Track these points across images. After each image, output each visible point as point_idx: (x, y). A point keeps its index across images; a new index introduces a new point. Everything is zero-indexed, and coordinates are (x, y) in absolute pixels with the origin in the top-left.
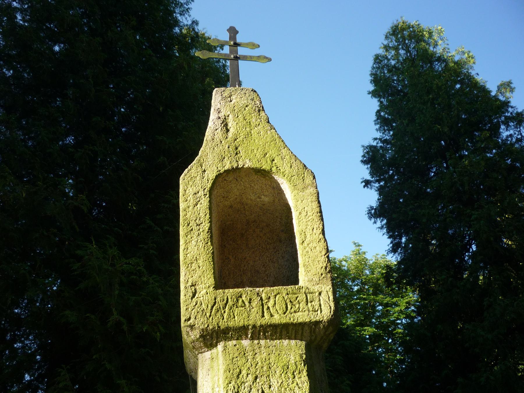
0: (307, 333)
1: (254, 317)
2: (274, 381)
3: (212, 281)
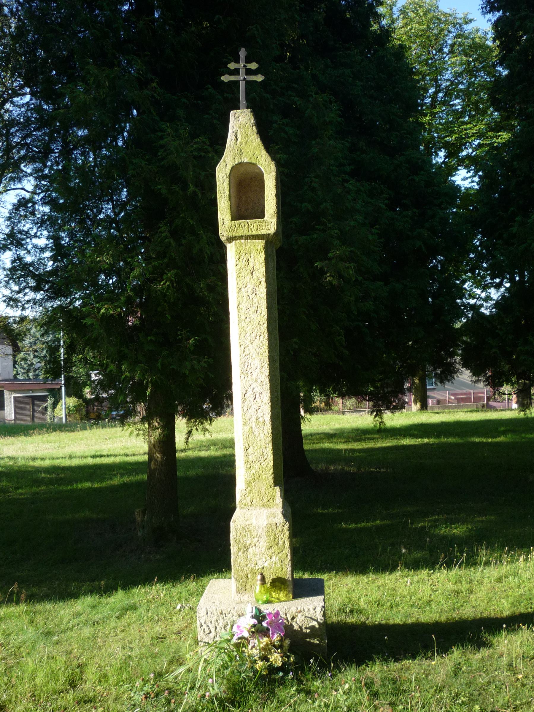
0: (265, 238)
1: (246, 233)
2: (252, 255)
3: (230, 218)
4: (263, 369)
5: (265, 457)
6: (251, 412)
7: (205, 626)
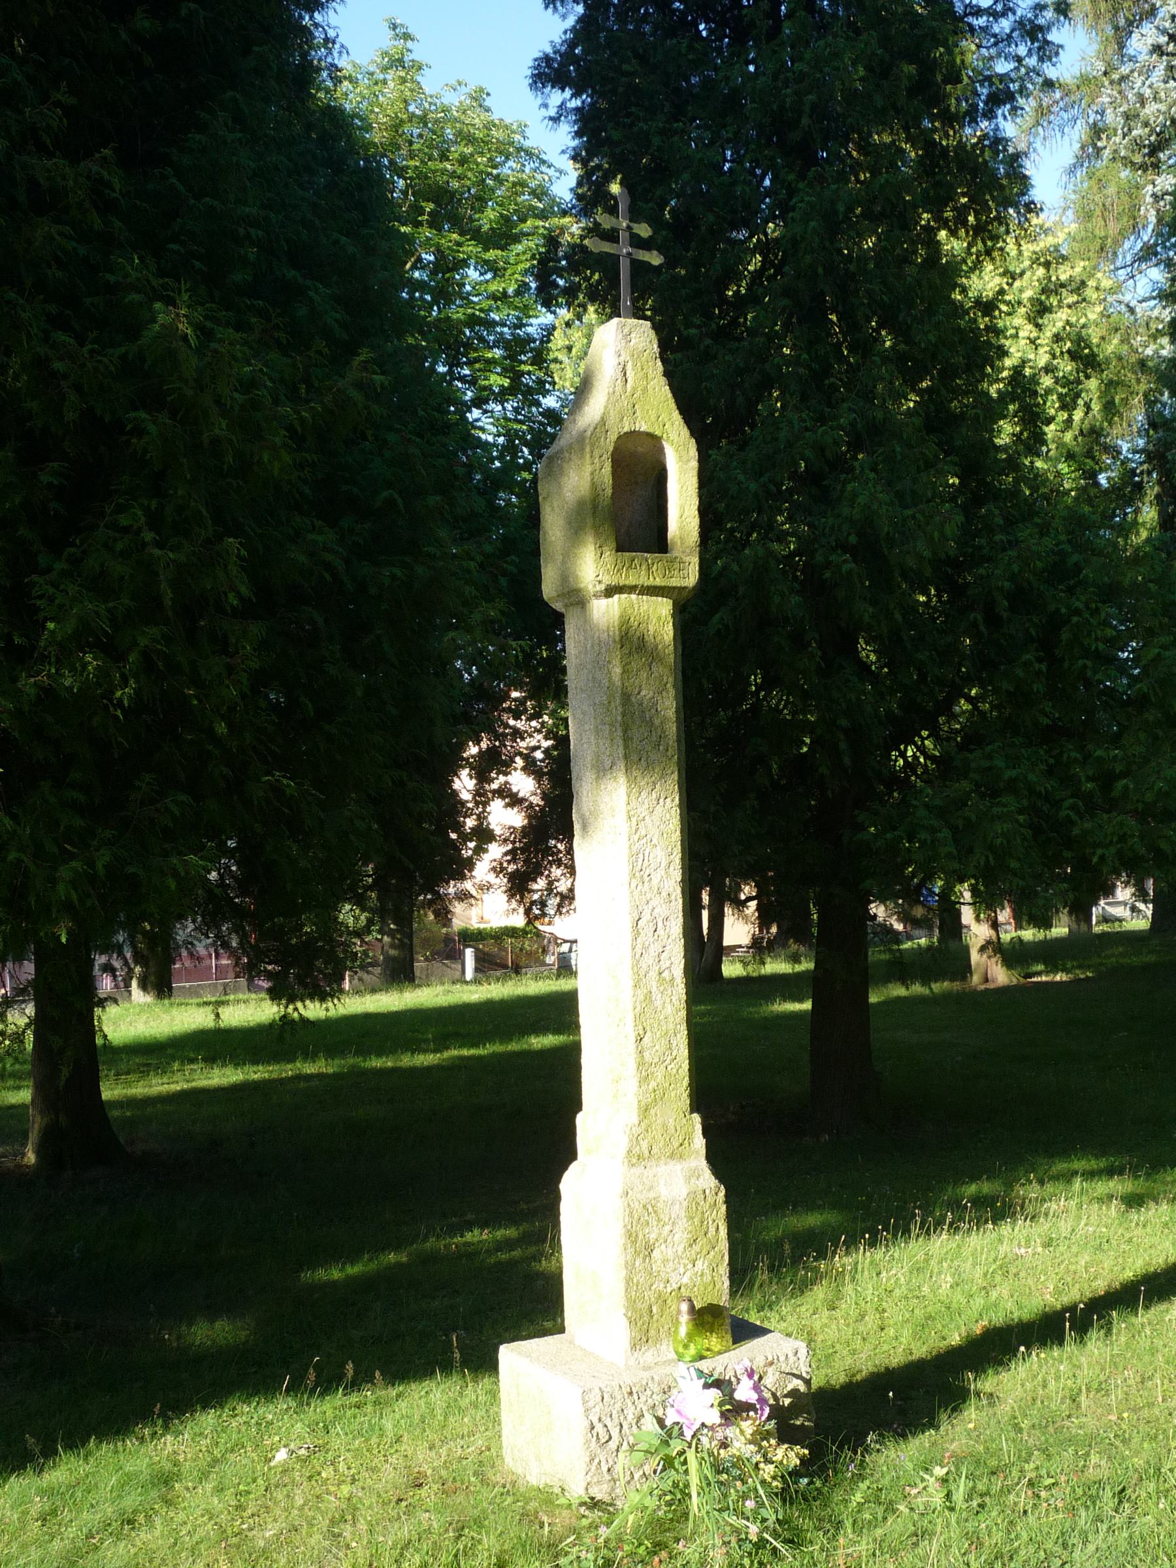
4: (672, 868)
6: (649, 959)
7: (599, 1428)
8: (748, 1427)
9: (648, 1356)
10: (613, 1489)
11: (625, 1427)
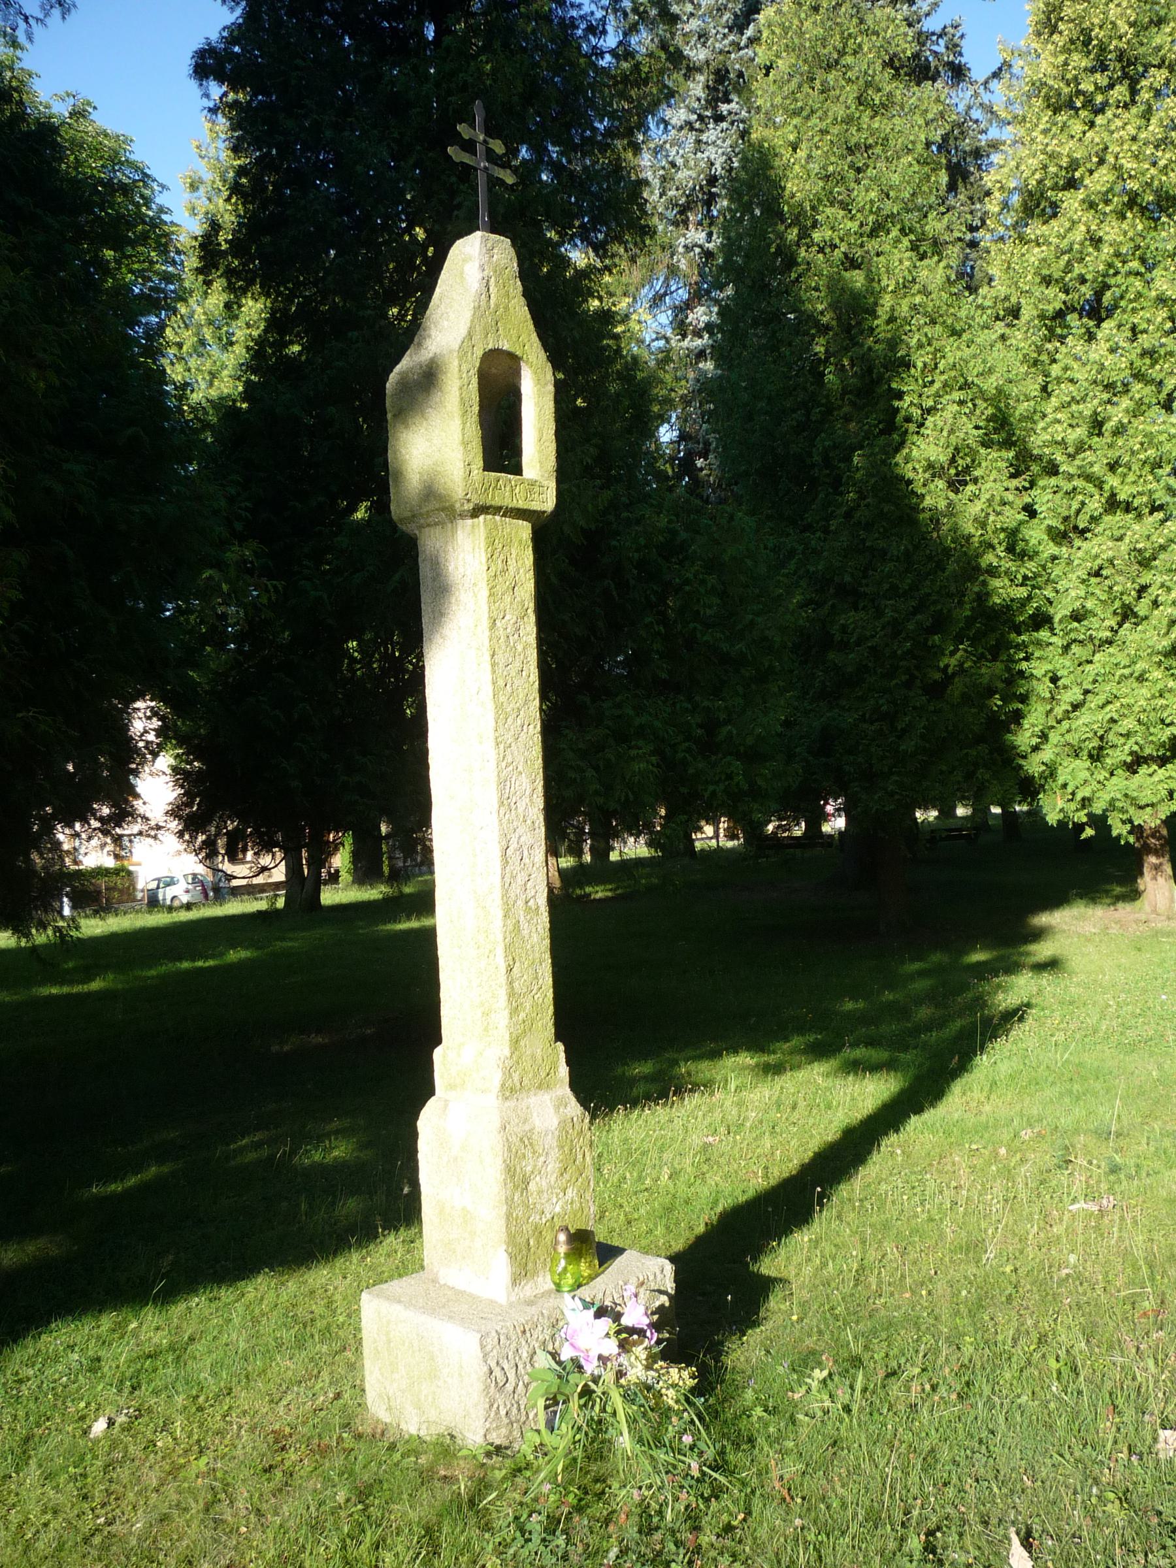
3: (481, 464)
5: (541, 982)
6: (516, 889)
7: (497, 1372)
8: (640, 1352)
9: (528, 1290)
10: (511, 1432)
11: (520, 1366)
